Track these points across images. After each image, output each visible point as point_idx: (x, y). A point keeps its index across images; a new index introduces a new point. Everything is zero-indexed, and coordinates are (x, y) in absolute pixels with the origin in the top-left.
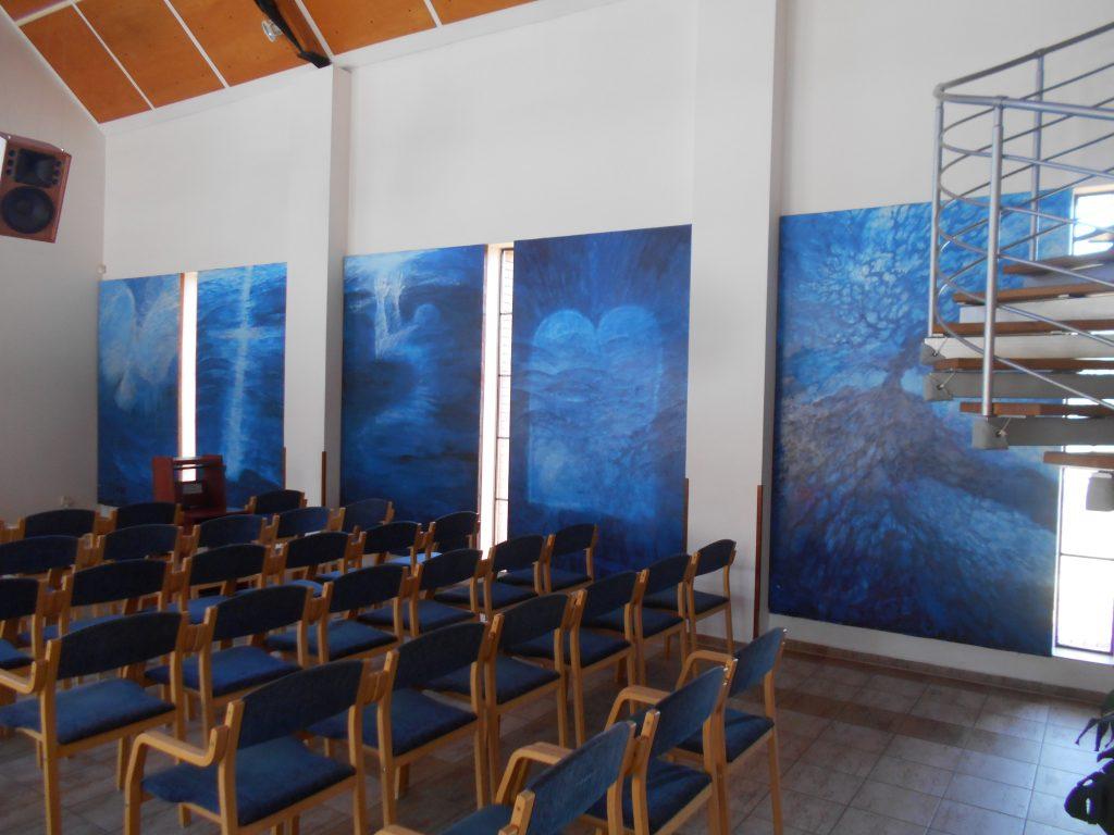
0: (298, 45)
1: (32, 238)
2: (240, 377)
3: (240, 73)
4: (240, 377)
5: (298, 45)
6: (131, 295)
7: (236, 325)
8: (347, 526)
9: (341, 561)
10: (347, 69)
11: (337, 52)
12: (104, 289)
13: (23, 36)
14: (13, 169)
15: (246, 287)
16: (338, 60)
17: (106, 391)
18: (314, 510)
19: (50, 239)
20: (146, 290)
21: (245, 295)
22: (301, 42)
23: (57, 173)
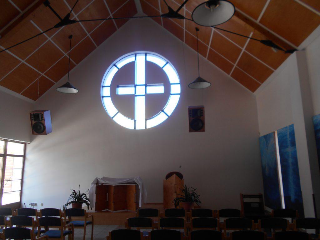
0: (283, 50)
1: (199, 131)
2: (290, 164)
3: (276, 65)
4: (290, 164)
5: (283, 50)
6: (265, 140)
7: (287, 147)
8: (76, 199)
9: (93, 210)
10: (304, 50)
11: (298, 45)
12: (260, 139)
13: (232, 78)
14: (151, 118)
15: (288, 133)
16: (300, 47)
17: (263, 169)
18: (284, 209)
19: (204, 131)
20: (268, 138)
21: (288, 136)
22: (284, 49)
23: (202, 113)
